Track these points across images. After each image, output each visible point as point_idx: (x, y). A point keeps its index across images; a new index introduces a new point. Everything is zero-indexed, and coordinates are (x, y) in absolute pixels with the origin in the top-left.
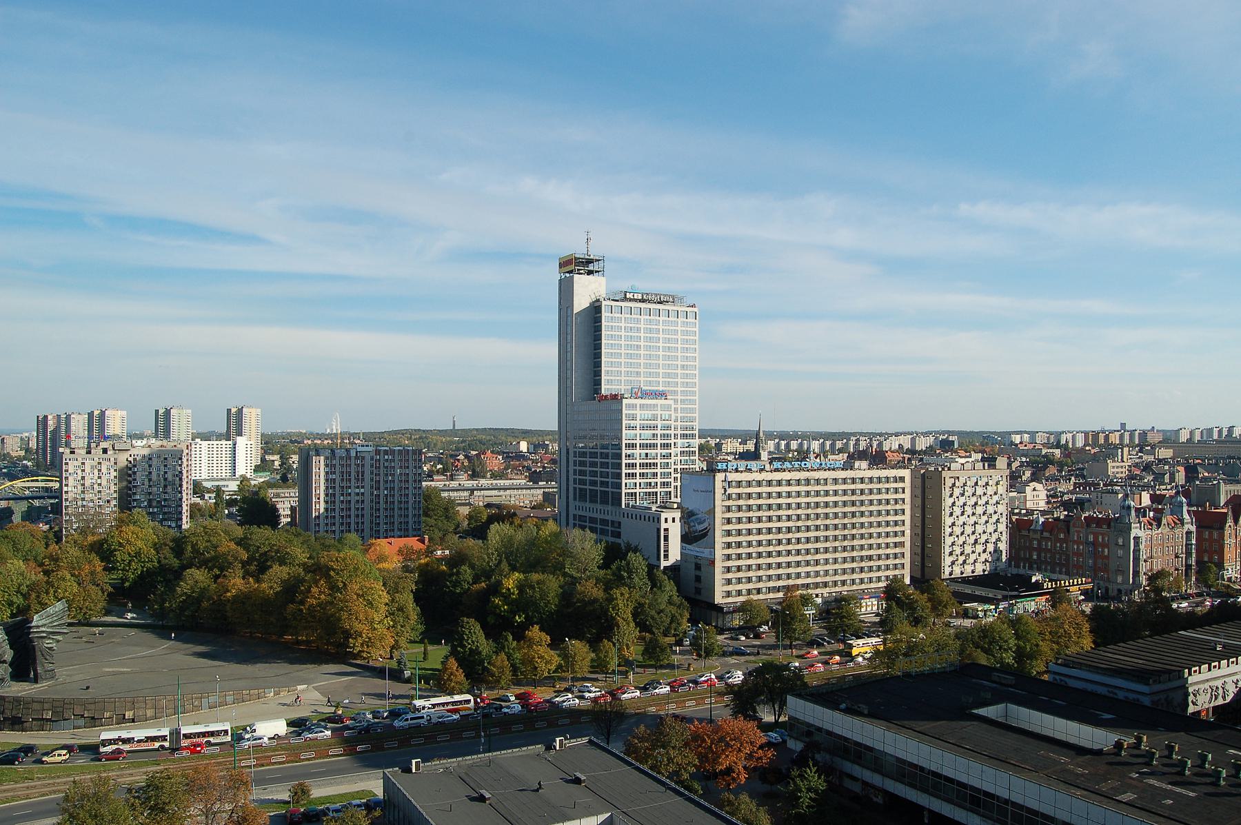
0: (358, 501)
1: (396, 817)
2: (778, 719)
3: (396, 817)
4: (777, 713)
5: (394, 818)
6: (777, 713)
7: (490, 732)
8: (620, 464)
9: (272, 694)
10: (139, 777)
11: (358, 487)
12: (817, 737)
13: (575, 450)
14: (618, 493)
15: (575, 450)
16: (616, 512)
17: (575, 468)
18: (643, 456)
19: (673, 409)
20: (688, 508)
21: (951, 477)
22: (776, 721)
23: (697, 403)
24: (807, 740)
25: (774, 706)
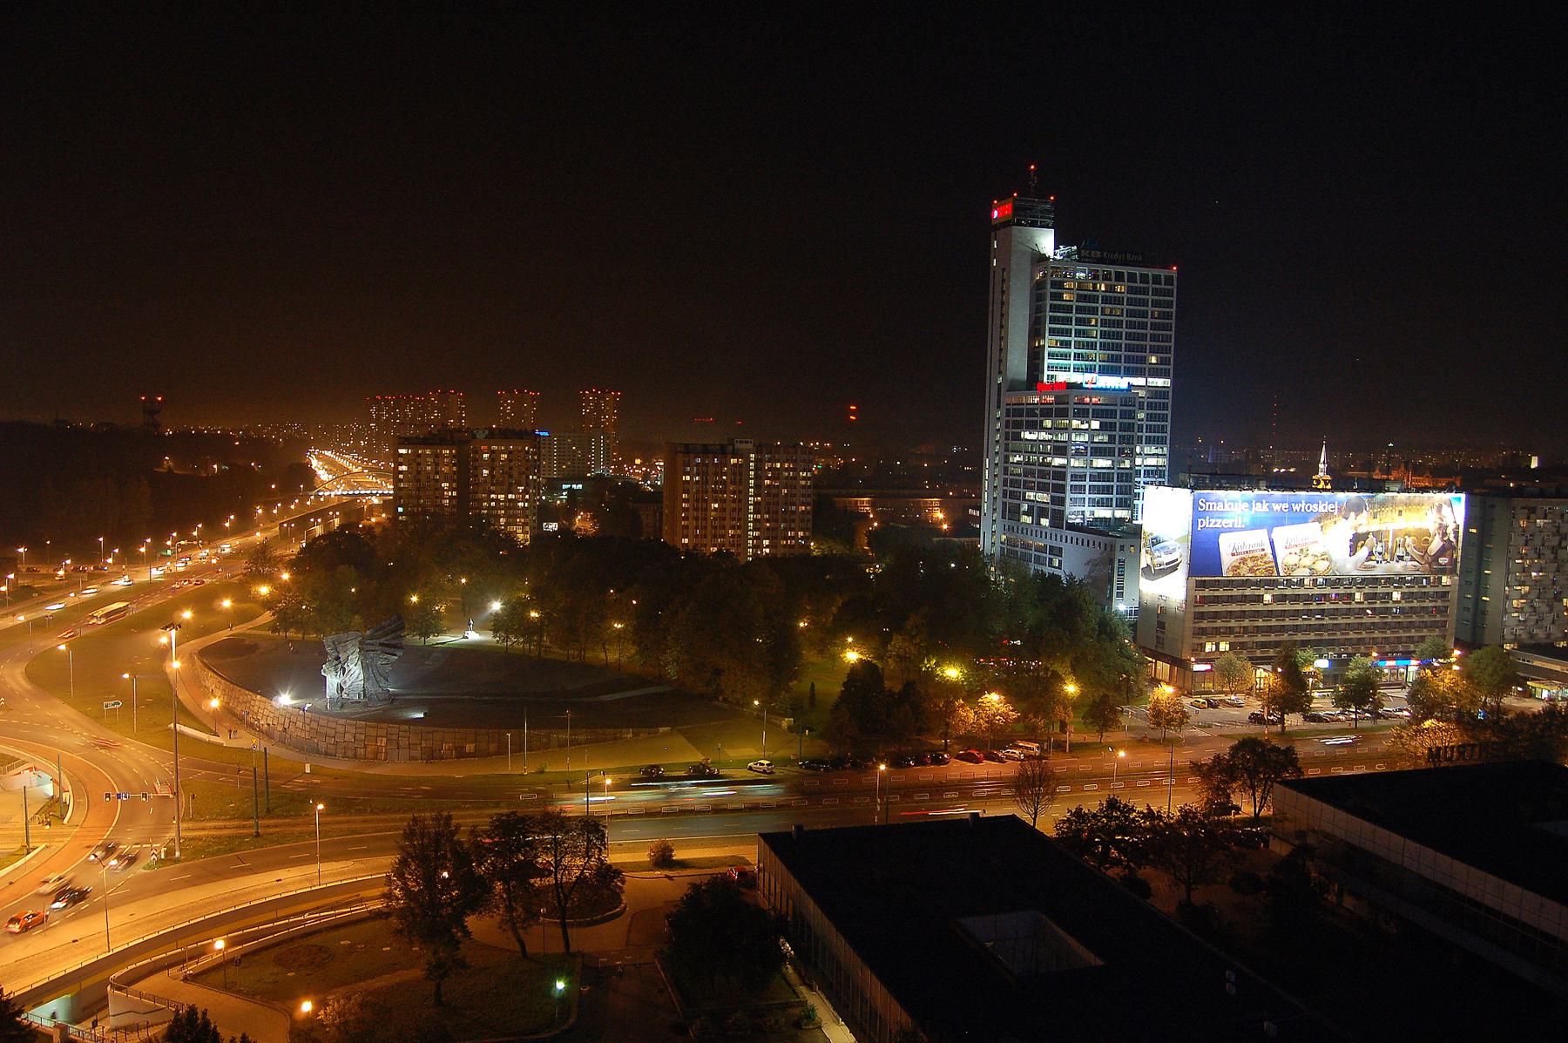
0: (734, 510)
1: (773, 890)
2: (1260, 811)
3: (773, 890)
4: (1258, 804)
5: (769, 891)
6: (1258, 804)
7: (887, 799)
8: (1063, 499)
9: (630, 735)
10: (481, 820)
11: (734, 519)
12: (1311, 840)
13: (1008, 407)
14: (1062, 485)
15: (1008, 407)
16: (1056, 536)
17: (1005, 488)
18: (1108, 312)
19: (1137, 404)
20: (1151, 534)
21: (1522, 508)
22: (1257, 815)
23: (1172, 363)
24: (1297, 842)
25: (1254, 795)
